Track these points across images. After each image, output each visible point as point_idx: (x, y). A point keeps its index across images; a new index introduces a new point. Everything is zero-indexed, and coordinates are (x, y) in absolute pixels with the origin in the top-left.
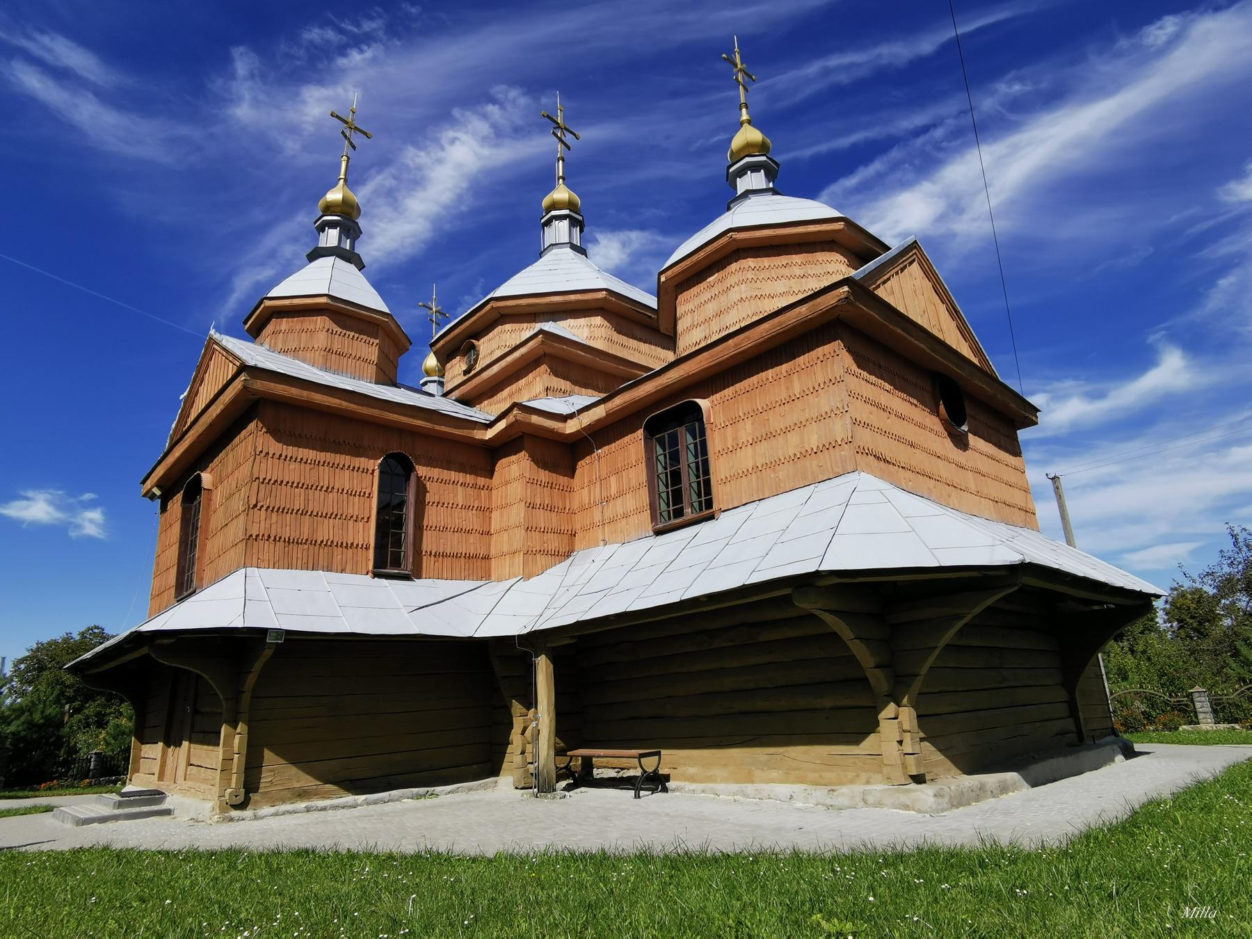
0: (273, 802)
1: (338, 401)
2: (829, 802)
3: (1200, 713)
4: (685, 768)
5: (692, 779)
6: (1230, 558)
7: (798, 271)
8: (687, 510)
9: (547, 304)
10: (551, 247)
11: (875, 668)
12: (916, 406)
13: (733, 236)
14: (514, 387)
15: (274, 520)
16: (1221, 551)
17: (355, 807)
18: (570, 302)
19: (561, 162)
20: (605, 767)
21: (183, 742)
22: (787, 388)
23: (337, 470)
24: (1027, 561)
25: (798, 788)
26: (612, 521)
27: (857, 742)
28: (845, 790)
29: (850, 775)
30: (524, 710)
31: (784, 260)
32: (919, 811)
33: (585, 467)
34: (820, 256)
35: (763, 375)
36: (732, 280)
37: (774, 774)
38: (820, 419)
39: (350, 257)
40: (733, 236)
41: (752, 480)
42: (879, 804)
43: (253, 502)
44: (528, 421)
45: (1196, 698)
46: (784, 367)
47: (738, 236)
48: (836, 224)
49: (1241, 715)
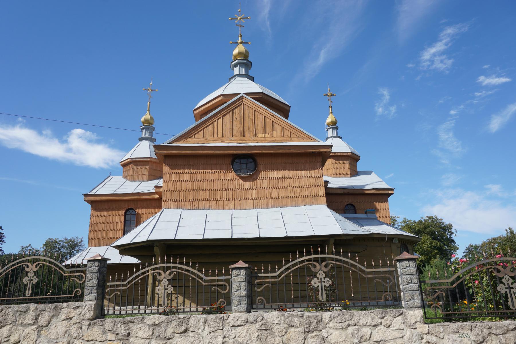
15: (96, 234)
23: (317, 179)
43: (90, 230)
44: (159, 191)
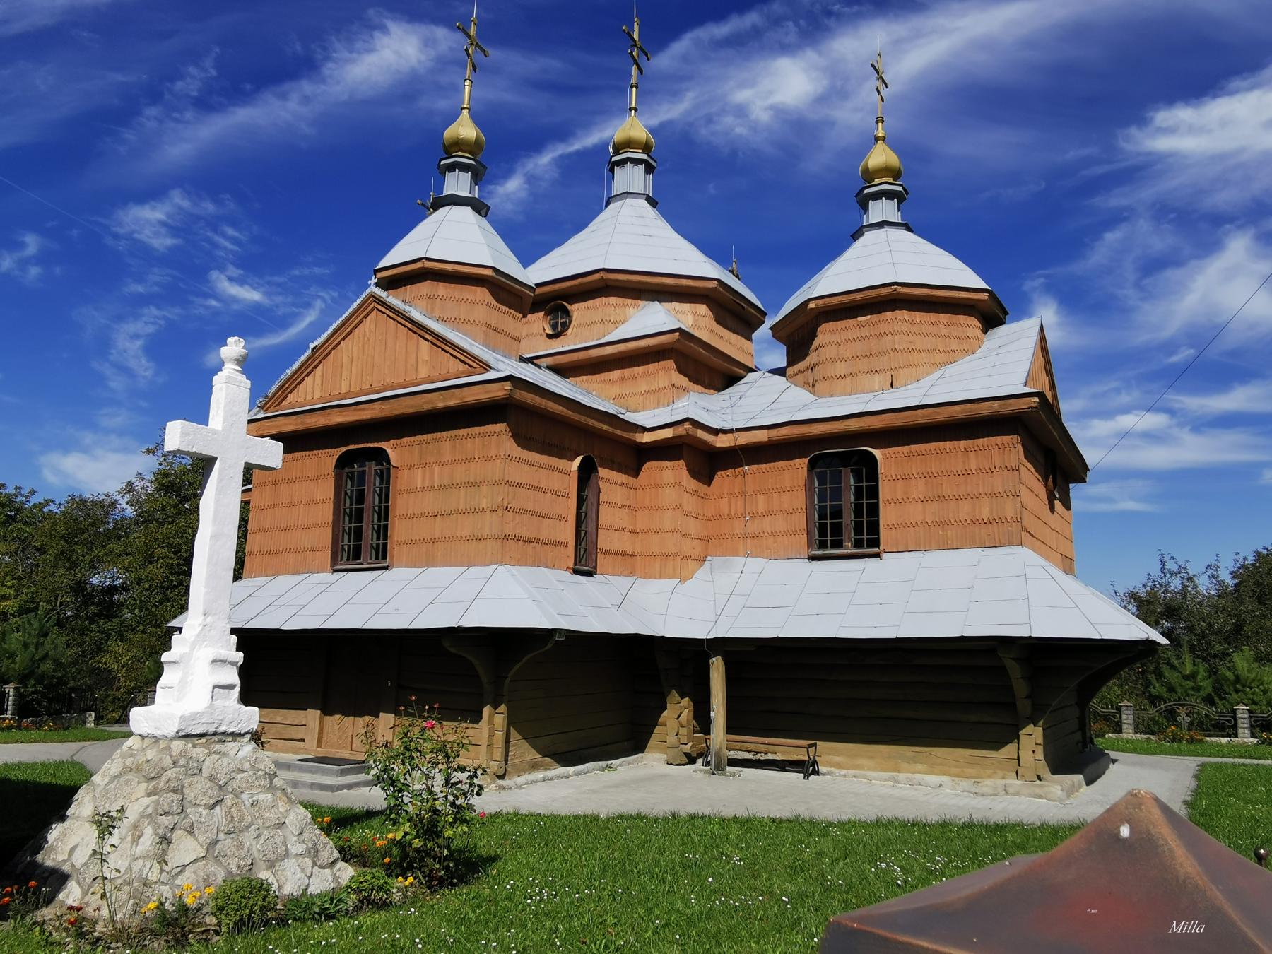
0: (519, 772)
1: (561, 408)
2: (974, 790)
3: (1125, 723)
4: (831, 757)
5: (839, 766)
6: (1154, 581)
7: (944, 331)
8: (847, 544)
9: (658, 285)
10: (626, 195)
11: (1025, 698)
12: (1039, 480)
13: (898, 290)
14: (626, 372)
16: (1149, 575)
17: (567, 777)
18: (681, 287)
19: (634, 89)
20: (738, 750)
21: (381, 714)
22: (964, 462)
24: (1150, 639)
25: (945, 779)
26: (757, 536)
27: (997, 749)
28: (988, 782)
29: (988, 772)
30: (679, 699)
31: (932, 317)
32: (1050, 800)
33: (724, 479)
34: (962, 319)
35: (941, 444)
36: (884, 328)
37: (920, 767)
38: (994, 496)
39: (479, 207)
40: (898, 290)
41: (919, 531)
42: (1018, 794)
45: (1124, 711)
46: (963, 443)
47: (901, 290)
48: (982, 294)
49: (1155, 728)
